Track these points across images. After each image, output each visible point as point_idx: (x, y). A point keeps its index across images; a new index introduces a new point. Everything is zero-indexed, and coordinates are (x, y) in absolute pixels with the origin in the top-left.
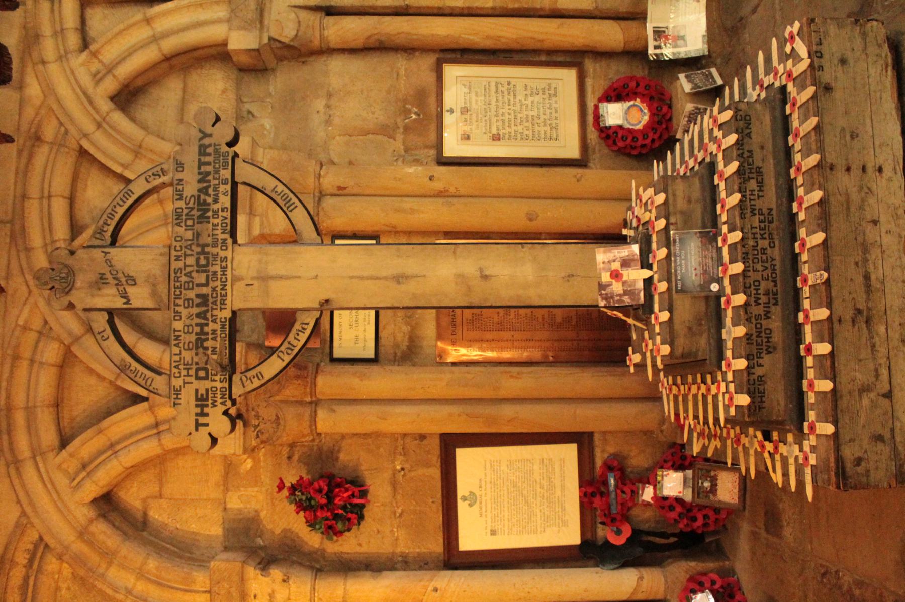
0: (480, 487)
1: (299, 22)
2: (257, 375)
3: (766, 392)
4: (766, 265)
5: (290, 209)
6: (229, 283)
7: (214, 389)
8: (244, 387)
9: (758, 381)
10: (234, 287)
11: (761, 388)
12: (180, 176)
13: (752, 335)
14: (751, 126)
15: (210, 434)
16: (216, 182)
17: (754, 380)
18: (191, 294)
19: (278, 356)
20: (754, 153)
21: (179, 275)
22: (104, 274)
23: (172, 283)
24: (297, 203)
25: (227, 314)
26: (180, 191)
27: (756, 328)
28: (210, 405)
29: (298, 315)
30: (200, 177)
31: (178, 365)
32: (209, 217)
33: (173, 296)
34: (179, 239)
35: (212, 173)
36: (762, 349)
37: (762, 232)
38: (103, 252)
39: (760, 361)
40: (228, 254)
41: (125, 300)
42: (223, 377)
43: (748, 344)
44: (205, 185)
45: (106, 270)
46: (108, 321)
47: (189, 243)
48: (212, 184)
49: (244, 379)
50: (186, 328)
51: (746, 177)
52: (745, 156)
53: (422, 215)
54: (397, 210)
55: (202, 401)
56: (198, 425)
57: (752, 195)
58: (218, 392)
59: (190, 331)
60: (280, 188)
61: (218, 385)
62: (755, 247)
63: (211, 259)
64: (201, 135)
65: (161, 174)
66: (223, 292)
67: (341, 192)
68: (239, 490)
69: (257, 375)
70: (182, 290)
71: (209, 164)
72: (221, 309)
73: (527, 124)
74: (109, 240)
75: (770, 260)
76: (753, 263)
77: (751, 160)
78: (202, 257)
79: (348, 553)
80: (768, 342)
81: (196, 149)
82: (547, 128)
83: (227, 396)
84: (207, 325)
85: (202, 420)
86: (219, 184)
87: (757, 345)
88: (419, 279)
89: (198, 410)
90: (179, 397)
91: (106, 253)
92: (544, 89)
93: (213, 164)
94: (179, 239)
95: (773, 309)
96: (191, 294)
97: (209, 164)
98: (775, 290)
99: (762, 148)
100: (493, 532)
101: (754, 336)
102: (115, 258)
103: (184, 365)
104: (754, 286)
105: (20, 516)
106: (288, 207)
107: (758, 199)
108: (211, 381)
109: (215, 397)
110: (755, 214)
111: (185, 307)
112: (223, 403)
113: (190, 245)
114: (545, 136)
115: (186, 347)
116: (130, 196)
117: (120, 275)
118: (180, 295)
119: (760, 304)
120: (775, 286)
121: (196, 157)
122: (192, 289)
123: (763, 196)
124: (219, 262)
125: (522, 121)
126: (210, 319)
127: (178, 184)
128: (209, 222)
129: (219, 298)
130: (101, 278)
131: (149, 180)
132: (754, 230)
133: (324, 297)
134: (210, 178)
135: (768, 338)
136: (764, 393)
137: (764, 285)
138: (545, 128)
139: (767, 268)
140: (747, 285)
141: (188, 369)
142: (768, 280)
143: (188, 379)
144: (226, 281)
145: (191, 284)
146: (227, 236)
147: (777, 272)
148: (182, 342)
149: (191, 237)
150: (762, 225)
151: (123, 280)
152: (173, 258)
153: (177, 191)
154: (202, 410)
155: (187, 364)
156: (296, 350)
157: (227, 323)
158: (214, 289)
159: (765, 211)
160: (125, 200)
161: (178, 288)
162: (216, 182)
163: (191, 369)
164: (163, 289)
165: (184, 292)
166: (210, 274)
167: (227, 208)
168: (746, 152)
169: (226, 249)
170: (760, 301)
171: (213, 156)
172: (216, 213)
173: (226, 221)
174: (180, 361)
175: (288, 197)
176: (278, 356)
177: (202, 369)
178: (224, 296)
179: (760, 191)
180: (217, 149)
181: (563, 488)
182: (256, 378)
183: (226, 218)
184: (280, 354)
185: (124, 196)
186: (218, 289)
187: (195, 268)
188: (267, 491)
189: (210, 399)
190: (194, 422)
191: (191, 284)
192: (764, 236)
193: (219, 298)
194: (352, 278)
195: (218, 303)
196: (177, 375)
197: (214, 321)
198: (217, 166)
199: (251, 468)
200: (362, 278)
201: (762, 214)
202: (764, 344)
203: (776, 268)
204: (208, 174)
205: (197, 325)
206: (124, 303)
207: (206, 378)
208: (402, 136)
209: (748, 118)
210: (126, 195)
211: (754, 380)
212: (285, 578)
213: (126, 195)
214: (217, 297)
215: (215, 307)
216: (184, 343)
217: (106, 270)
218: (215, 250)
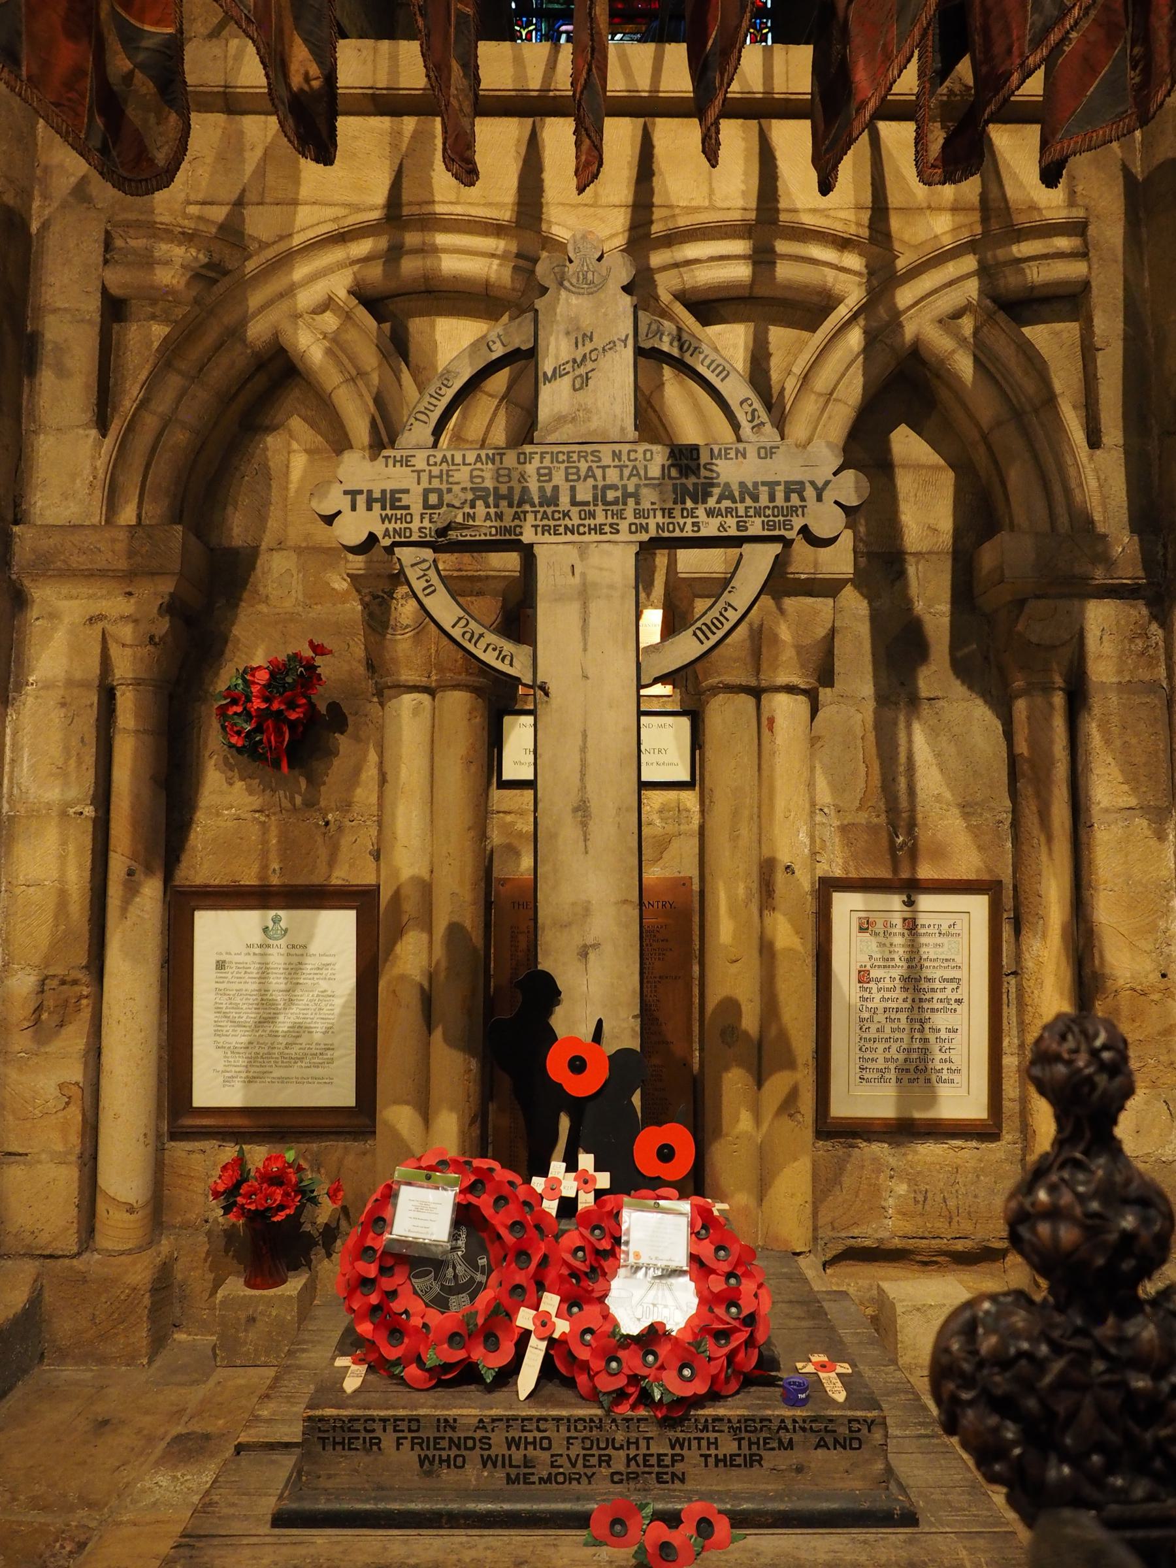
0: (293, 947)
1: (1054, 647)
2: (431, 585)
3: (353, 1453)
4: (580, 1462)
5: (699, 633)
6: (576, 538)
7: (409, 519)
8: (412, 566)
9: (371, 1439)
10: (570, 547)
11: (358, 1444)
12: (751, 452)
13: (453, 1429)
14: (839, 1448)
15: (339, 512)
16: (741, 512)
17: (373, 1431)
18: (558, 478)
19: (460, 619)
20: (789, 1451)
21: (590, 458)
22: (591, 340)
23: (577, 448)
24: (708, 644)
25: (528, 536)
26: (726, 454)
27: (466, 1438)
28: (384, 513)
29: (527, 649)
30: (750, 486)
31: (447, 462)
32: (684, 502)
33: (556, 449)
34: (648, 455)
35: (757, 505)
36: (428, 1449)
37: (640, 1459)
38: (627, 336)
39: (407, 1444)
40: (624, 536)
41: (549, 375)
42: (427, 531)
43: (439, 1420)
44: (737, 494)
45: (598, 342)
46: (518, 350)
47: (642, 473)
48: (738, 505)
49: (425, 566)
50: (506, 472)
51: (743, 1435)
52: (782, 1433)
53: (727, 854)
54: (735, 813)
55: (391, 501)
56: (353, 494)
57: (709, 1443)
58: (405, 525)
59: (501, 479)
60: (733, 616)
61: (415, 525)
62: (611, 1442)
63: (615, 508)
64: (820, 484)
65: (755, 423)
66: (562, 530)
67: (764, 722)
68: (299, 571)
69: (431, 585)
70: (566, 464)
71: (772, 498)
72: (536, 527)
73: (888, 1029)
74: (647, 345)
75: (589, 1472)
76: (584, 1438)
77: (775, 1445)
78: (619, 494)
79: (199, 738)
80: (441, 1461)
81: (797, 478)
82: (881, 1064)
83: (397, 539)
84: (510, 505)
85: (361, 501)
86: (737, 516)
87: (435, 1438)
88: (581, 844)
89: (377, 494)
90: (398, 464)
91: (625, 341)
92: (951, 1061)
93: (771, 505)
94: (648, 455)
95: (500, 1474)
96: (558, 478)
97: (772, 498)
98: (535, 1479)
99: (799, 1469)
100: (221, 965)
101: (449, 1434)
102: (617, 357)
103: (448, 471)
104: (542, 1438)
105: (260, 242)
106: (700, 629)
107: (701, 1455)
108: (422, 514)
109: (396, 519)
110: (673, 1448)
111: (539, 469)
112: (386, 533)
113: (638, 474)
114: (867, 1060)
115: (475, 473)
116: (717, 376)
117: (590, 365)
118: (558, 462)
119: (509, 1449)
120: (541, 1479)
121: (782, 479)
122: (567, 480)
123: (706, 1466)
124: (610, 520)
125: (893, 1021)
126: (519, 510)
127: (737, 451)
128: (675, 503)
129: (552, 523)
130: (585, 335)
131: (745, 405)
132: (643, 1444)
133: (553, 688)
134: (749, 502)
135: (448, 1460)
136: (350, 1449)
137: (545, 1456)
138: (881, 1060)
139: (574, 1465)
140: (542, 1425)
141: (441, 477)
142: (553, 1466)
143: (425, 477)
144: (579, 534)
145: (575, 477)
146: (653, 532)
147: (566, 1486)
148: (484, 467)
149: (650, 475)
150: (653, 1461)
151: (582, 370)
152: (617, 447)
153: (726, 449)
154: (376, 500)
155: (448, 476)
156: (470, 647)
157: (513, 537)
158: (566, 514)
159: (679, 1467)
160: (712, 368)
161: (569, 457)
162: (741, 512)
163: (441, 481)
164: (567, 432)
165: (563, 466)
166: (592, 508)
167: (699, 531)
168: (788, 1436)
169: (631, 532)
170: (513, 1448)
171: (785, 505)
172: (692, 514)
173: (677, 529)
174: (453, 464)
175: (718, 628)
176: (460, 619)
177: (441, 498)
178: (555, 530)
179: (717, 1461)
180: (796, 511)
181: (283, 1080)
182: (426, 584)
183: (682, 530)
184: (463, 622)
185: (718, 366)
186: (567, 522)
187: (600, 484)
188: (298, 614)
189: (394, 512)
190: (357, 488)
191: (575, 477)
192: (633, 1463)
193: (552, 523)
194: (585, 735)
195: (545, 522)
196: (432, 460)
197: (516, 516)
198: (768, 512)
199: (333, 589)
200: (583, 749)
201: (673, 1461)
202: (437, 1453)
203: (574, 1483)
204: (755, 498)
205: (511, 489)
206: (545, 374)
207: (426, 506)
208: (864, 822)
209: (855, 1444)
210: (720, 368)
211: (373, 1431)
212: (157, 640)
213: (720, 368)
214: (554, 519)
215: (539, 516)
216: (482, 470)
217: (598, 342)
218: (629, 513)
